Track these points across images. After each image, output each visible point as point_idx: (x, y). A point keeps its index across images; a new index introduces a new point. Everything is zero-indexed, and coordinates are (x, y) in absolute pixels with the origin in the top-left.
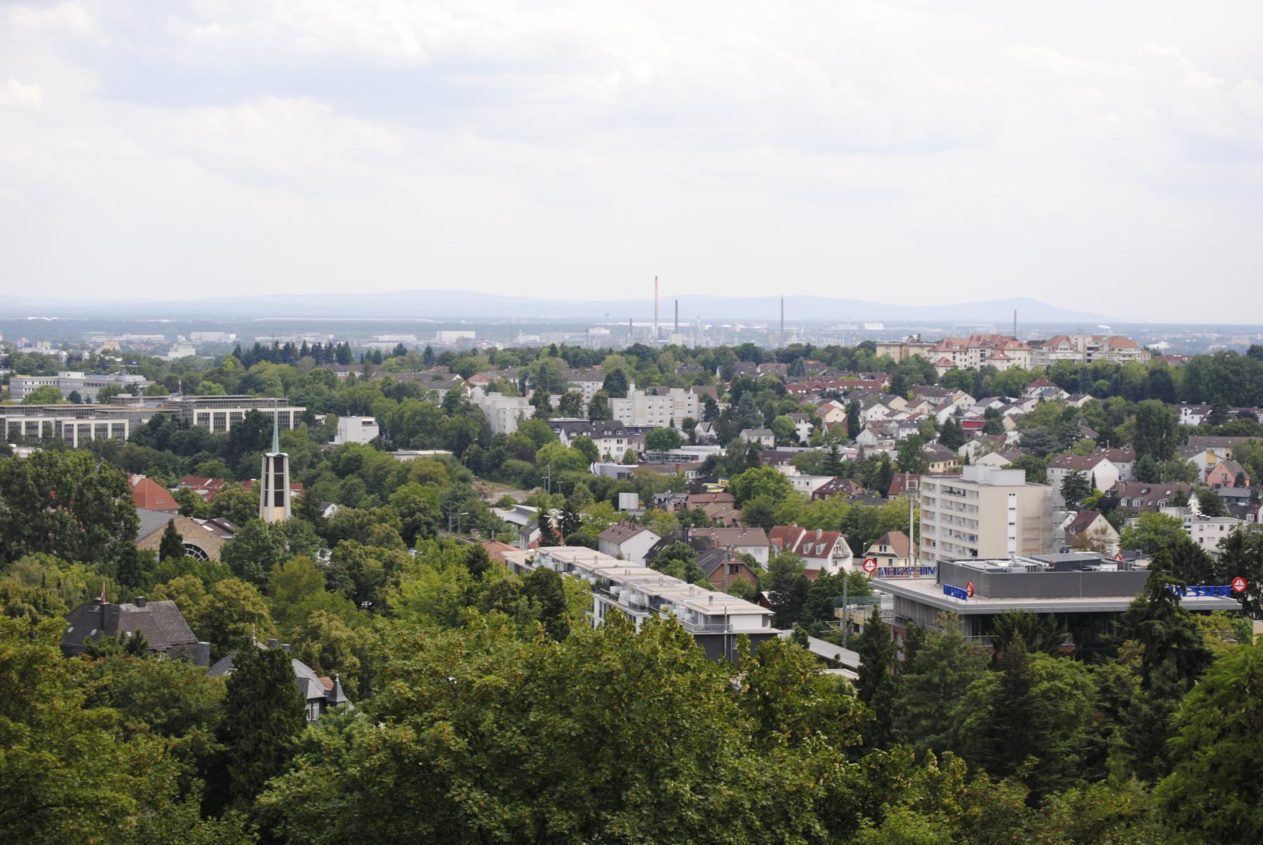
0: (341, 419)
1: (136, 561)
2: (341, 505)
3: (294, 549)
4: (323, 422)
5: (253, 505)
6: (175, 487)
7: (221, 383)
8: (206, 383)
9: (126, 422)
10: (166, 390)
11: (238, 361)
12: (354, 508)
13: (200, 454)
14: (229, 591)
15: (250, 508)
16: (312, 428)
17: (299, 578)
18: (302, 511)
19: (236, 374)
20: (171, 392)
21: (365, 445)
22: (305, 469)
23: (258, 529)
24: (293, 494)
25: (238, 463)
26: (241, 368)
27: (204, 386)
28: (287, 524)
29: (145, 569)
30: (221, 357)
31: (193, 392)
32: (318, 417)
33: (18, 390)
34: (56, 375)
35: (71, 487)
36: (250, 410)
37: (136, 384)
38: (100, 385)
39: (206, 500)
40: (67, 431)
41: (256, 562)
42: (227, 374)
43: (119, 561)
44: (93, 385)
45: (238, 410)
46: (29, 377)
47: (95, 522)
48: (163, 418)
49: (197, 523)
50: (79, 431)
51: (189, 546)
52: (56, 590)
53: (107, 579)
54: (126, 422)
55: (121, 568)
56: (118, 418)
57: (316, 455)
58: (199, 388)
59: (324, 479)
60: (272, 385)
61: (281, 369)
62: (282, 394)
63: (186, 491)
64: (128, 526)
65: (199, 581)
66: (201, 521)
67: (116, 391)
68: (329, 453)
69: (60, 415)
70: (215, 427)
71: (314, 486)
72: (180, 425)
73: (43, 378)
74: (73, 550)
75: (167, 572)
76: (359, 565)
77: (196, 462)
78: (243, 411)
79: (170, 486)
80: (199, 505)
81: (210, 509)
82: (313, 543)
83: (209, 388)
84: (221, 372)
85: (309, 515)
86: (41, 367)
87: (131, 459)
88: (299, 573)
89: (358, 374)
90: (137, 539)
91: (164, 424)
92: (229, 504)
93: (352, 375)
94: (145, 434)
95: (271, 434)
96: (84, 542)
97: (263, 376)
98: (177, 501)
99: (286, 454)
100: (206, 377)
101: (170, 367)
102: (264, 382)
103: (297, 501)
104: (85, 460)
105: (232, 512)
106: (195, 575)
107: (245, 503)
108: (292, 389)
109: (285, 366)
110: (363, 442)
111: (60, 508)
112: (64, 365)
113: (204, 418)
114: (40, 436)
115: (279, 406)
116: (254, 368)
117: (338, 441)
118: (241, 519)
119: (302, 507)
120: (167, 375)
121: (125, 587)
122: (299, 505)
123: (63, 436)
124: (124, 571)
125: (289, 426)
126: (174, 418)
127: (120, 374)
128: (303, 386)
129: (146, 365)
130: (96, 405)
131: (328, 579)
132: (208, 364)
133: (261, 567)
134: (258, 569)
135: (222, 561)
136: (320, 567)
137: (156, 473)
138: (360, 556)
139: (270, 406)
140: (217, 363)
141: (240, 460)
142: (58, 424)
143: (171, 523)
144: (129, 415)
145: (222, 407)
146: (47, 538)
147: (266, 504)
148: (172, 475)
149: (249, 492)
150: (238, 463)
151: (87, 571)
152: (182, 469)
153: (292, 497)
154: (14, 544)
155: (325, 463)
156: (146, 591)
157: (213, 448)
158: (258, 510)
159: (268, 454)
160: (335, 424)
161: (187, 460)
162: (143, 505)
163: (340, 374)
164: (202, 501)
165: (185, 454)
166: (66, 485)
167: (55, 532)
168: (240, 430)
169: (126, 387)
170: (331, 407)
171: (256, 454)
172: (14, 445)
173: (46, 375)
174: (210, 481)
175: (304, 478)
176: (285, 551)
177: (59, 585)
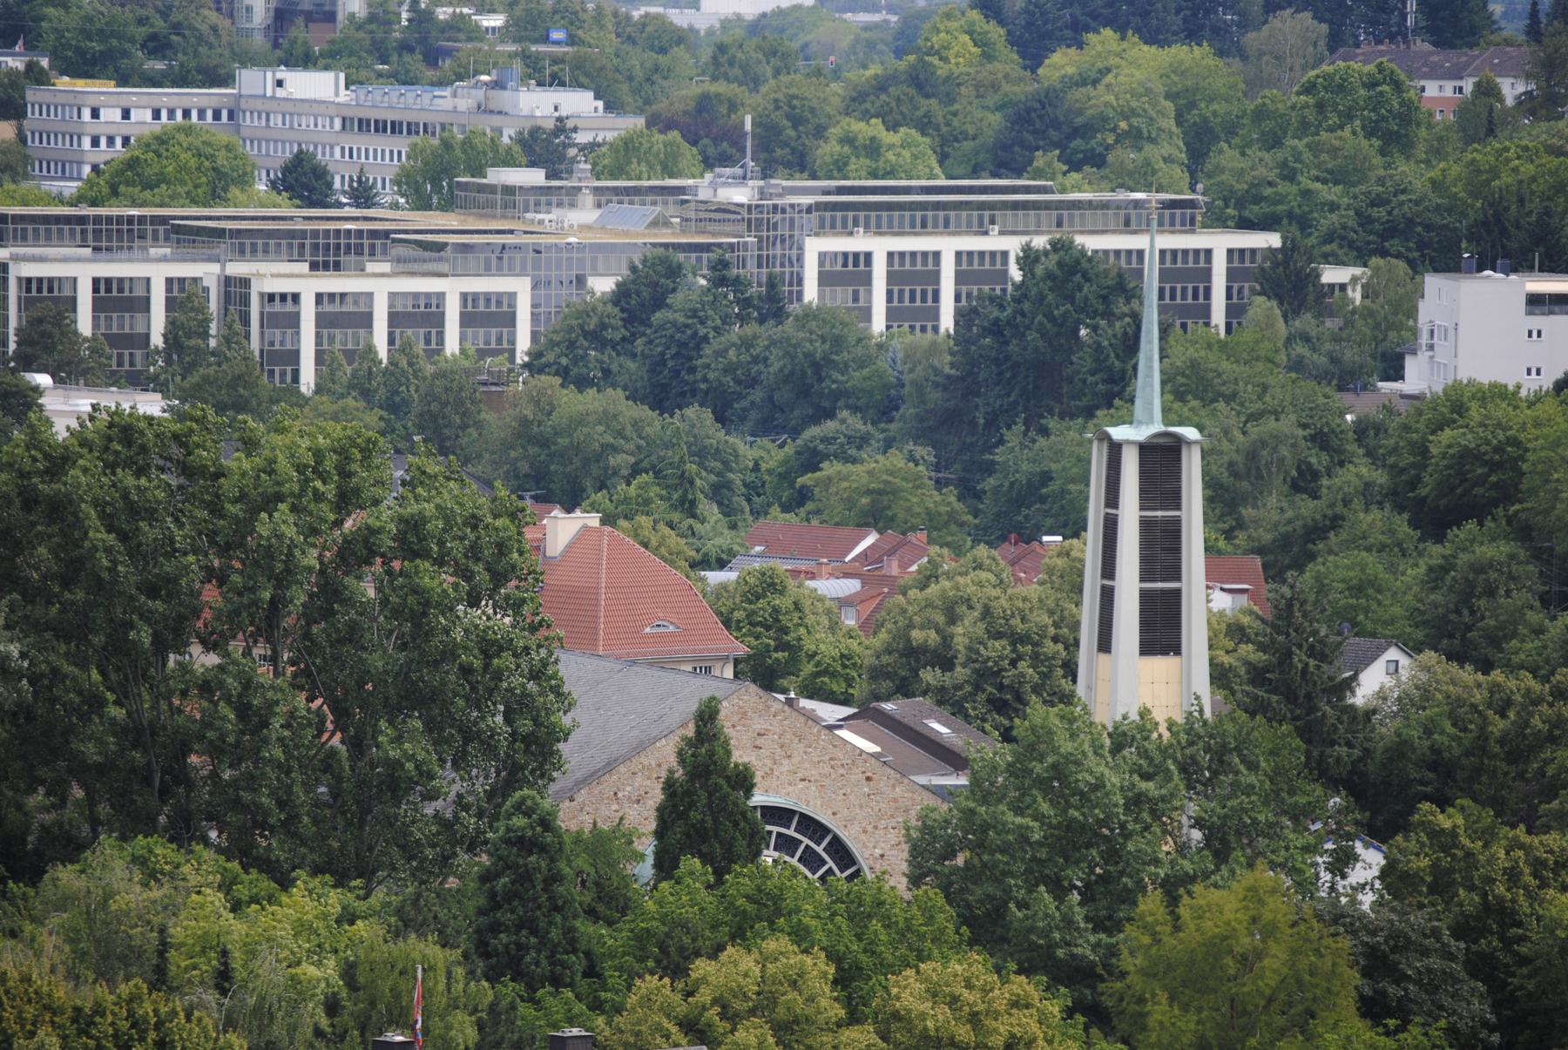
0: (1433, 283)
1: (556, 878)
2: (1429, 656)
3: (1220, 843)
4: (1356, 295)
5: (1049, 647)
6: (722, 564)
7: (924, 126)
8: (859, 128)
9: (520, 288)
10: (689, 154)
11: (996, 32)
12: (1486, 667)
13: (830, 426)
14: (943, 1013)
15: (1036, 659)
16: (1306, 322)
17: (1247, 962)
18: (1258, 675)
19: (983, 89)
20: (708, 163)
21: (1536, 400)
22: (1273, 500)
23: (1067, 747)
24: (1222, 601)
25: (989, 469)
26: (1009, 61)
27: (848, 140)
28: (1191, 731)
29: (591, 913)
30: (923, 16)
31: (801, 164)
32: (1332, 275)
33: (62, 144)
34: (226, 80)
35: (290, 568)
36: (1040, 242)
37: (562, 127)
38: (412, 129)
39: (850, 622)
40: (268, 320)
41: (1059, 889)
42: (948, 91)
43: (487, 877)
44: (381, 127)
45: (993, 242)
46: (110, 87)
47: (394, 712)
48: (674, 271)
49: (811, 717)
50: (322, 321)
51: (779, 815)
52: (211, 997)
53: (435, 953)
54: (520, 288)
55: (494, 902)
56: (487, 271)
57: (1321, 439)
58: (828, 149)
59: (1353, 543)
60: (1136, 137)
61: (1178, 69)
62: (1179, 174)
63: (770, 584)
64: (525, 725)
65: (818, 967)
66: (830, 712)
67: (478, 156)
68: (1379, 429)
69: (241, 253)
70: (891, 314)
71: (1311, 569)
72: (746, 303)
73: (168, 96)
74: (289, 825)
75: (684, 926)
76: (1504, 915)
77: (811, 460)
78: (1013, 245)
79: (704, 563)
80: (822, 644)
81: (869, 660)
82: (1300, 816)
83: (873, 149)
84: (920, 81)
85: (1290, 696)
86: (157, 46)
87: (544, 443)
88: (1245, 942)
89: (1511, 89)
90: (560, 782)
91: (676, 299)
92: (947, 640)
93: (1487, 91)
94: (596, 337)
95: (1131, 344)
96: (336, 794)
97: (1101, 99)
98: (727, 623)
99: (1190, 433)
100: (858, 103)
101: (706, 54)
102: (1101, 122)
103: (1237, 632)
104: (343, 452)
105: (961, 673)
106: (801, 936)
107: (1017, 639)
108: (1226, 157)
109: (1194, 56)
110: (1530, 385)
111: (236, 646)
112: (259, 41)
113: (851, 271)
114: (157, 340)
115: (1170, 226)
116: (1061, 63)
117: (1418, 377)
118: (999, 706)
119: (1259, 657)
120: (695, 90)
121: (510, 989)
122: (1247, 649)
123: (255, 343)
124: (505, 917)
125: (1206, 311)
126: (721, 275)
127: (498, 85)
128: (1273, 141)
129: (603, 44)
130: (395, 212)
131: (1366, 973)
132: (867, 45)
133: (1079, 914)
134: (1068, 922)
135: (915, 880)
136: (1340, 918)
137: (645, 505)
138: (1513, 876)
139: (1127, 226)
140: (904, 40)
141: (999, 455)
142: (236, 291)
143: (707, 716)
144: (533, 259)
145: (924, 228)
146: (180, 776)
147: (1105, 644)
148: (710, 510)
149: (1033, 590)
150: (989, 469)
151: (349, 917)
152: (752, 490)
153: (1214, 619)
154: (38, 798)
155: (1360, 471)
156: (597, 1006)
157: (884, 407)
158: (1071, 670)
159: (1118, 433)
160: (1407, 307)
161: (771, 454)
162: (586, 641)
163: (1432, 89)
164: (834, 626)
165: (766, 428)
166: (269, 553)
167: (216, 751)
168: (995, 329)
169: (520, 140)
170: (1390, 231)
171: (1064, 434)
172: (43, 380)
173: (181, 80)
174: (871, 539)
175: (1267, 537)
176: (1182, 849)
177: (223, 979)
